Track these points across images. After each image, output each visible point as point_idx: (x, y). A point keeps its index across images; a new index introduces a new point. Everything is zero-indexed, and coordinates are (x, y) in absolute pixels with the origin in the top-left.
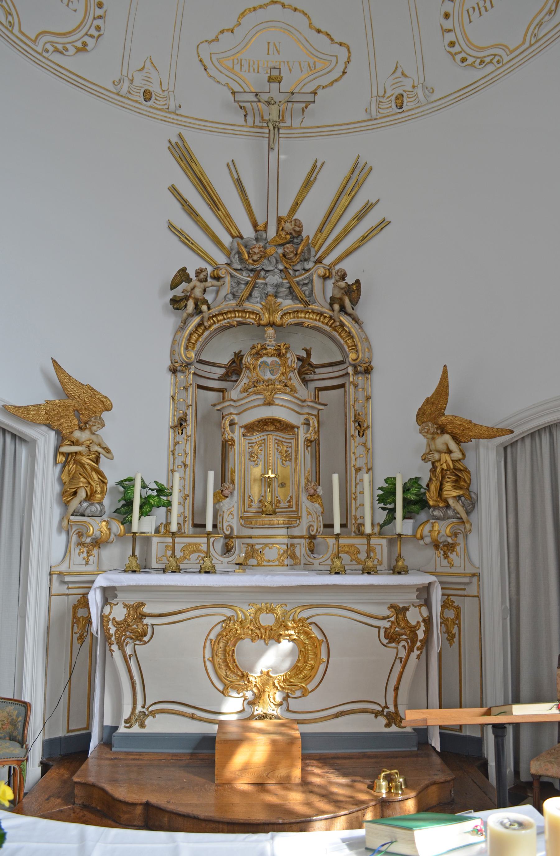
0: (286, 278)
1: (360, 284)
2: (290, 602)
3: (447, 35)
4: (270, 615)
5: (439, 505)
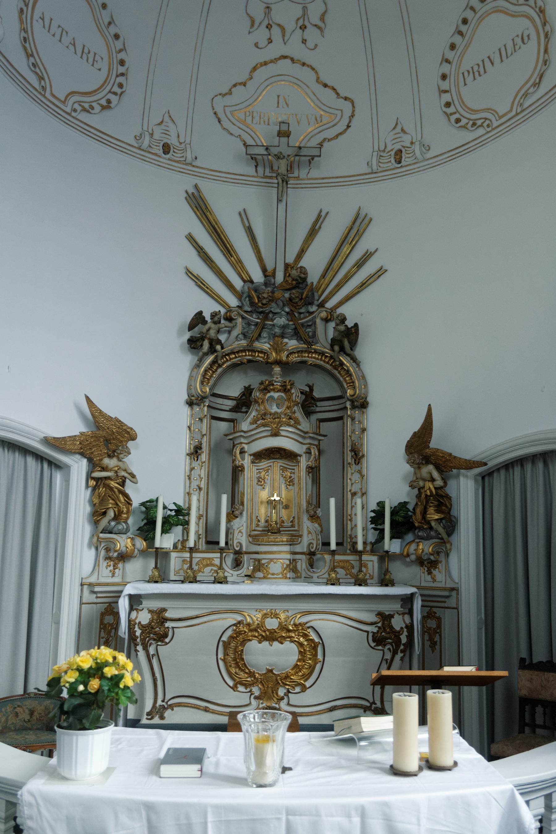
0: (292, 321)
2: (292, 609)
4: (274, 620)
5: (423, 527)
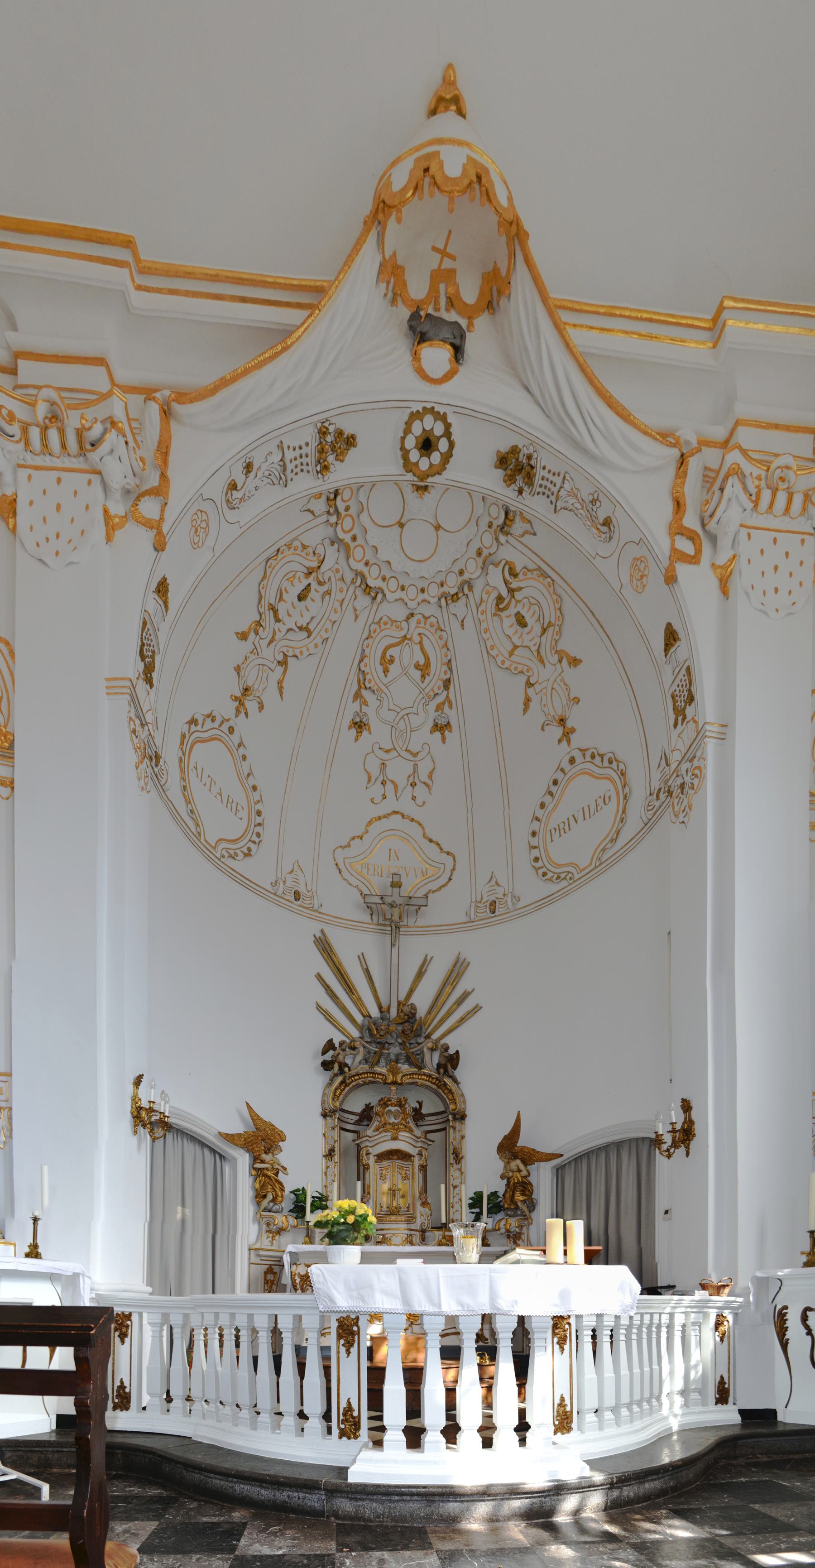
0: (404, 1050)
3: (533, 851)
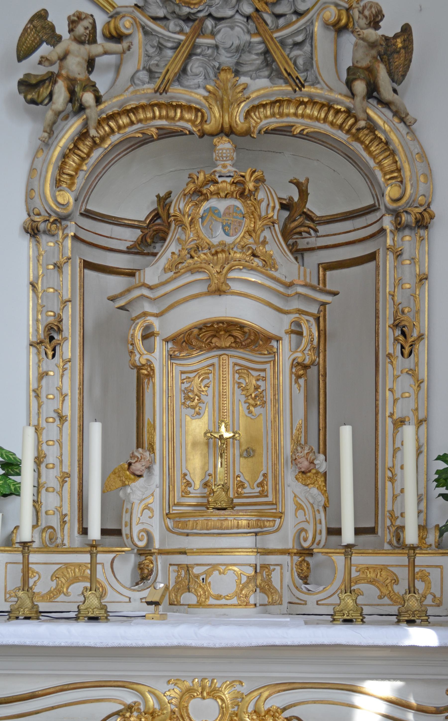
1: (411, 34)
4: (209, 702)
